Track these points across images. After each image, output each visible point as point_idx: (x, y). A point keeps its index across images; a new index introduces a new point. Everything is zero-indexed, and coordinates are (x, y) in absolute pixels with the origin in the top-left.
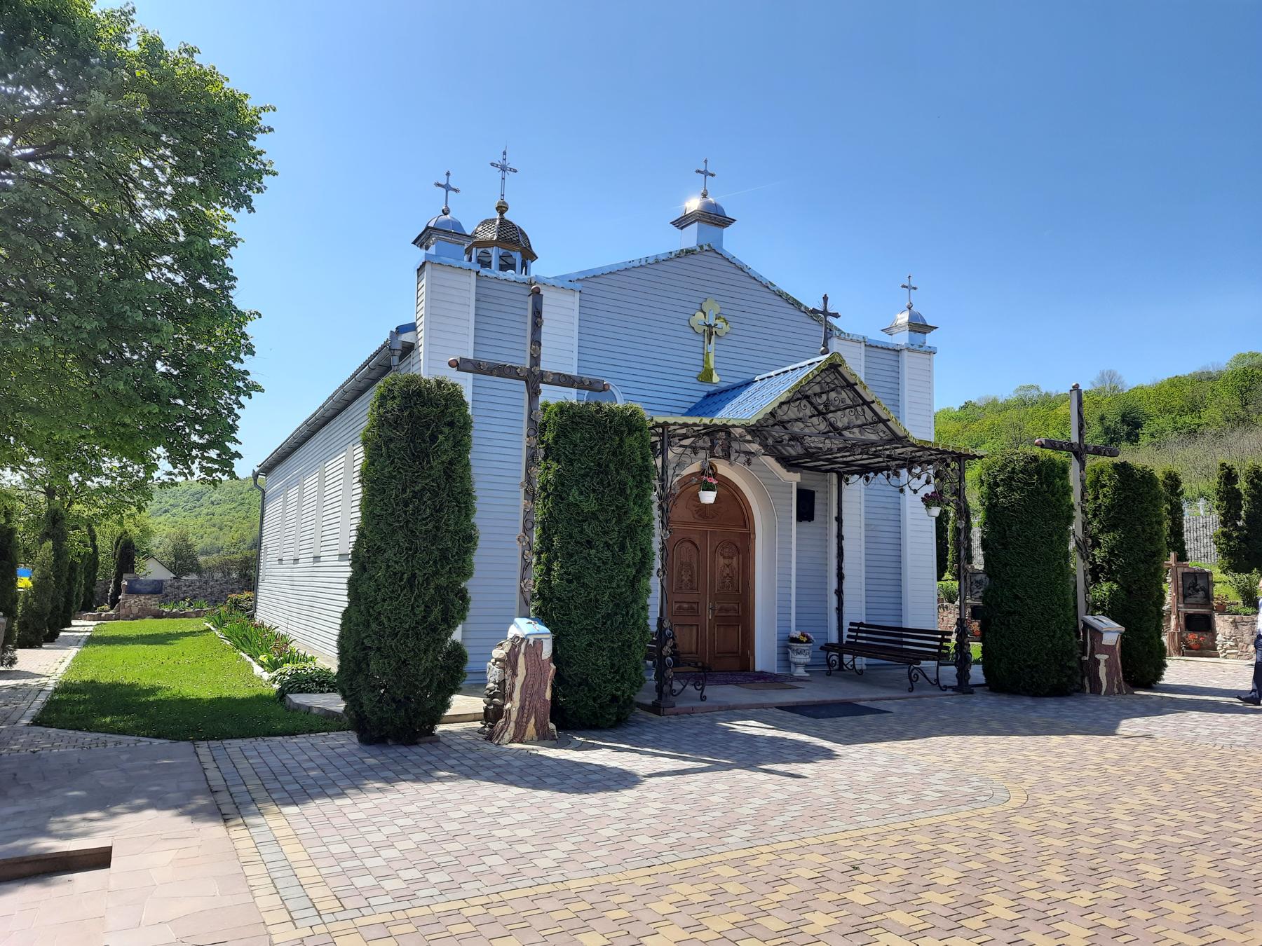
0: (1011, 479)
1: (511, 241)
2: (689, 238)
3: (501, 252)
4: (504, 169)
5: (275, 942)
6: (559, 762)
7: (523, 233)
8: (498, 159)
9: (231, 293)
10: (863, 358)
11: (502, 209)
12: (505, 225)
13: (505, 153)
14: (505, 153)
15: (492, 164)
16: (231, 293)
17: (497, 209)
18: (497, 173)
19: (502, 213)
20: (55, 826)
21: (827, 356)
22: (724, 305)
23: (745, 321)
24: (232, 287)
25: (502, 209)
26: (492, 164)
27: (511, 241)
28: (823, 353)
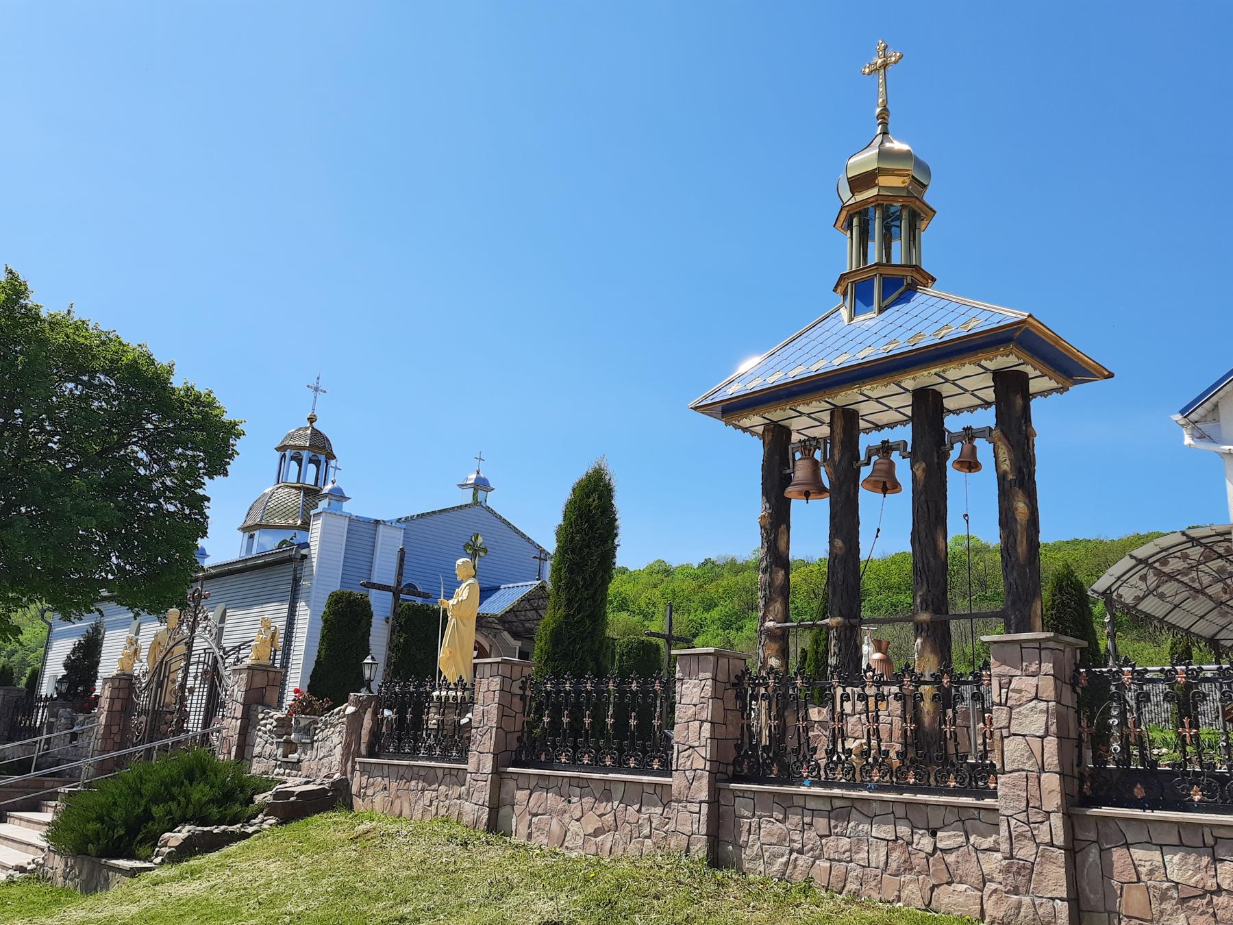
0: (630, 652)
1: (318, 448)
2: (466, 497)
3: (311, 454)
4: (316, 389)
5: (1132, 850)
6: (14, 742)
7: (328, 440)
8: (313, 383)
9: (227, 467)
10: (402, 539)
11: (312, 420)
12: (316, 433)
13: (318, 378)
14: (318, 378)
15: (308, 386)
16: (227, 467)
17: (308, 419)
18: (311, 392)
19: (311, 423)
20: (142, 851)
21: (540, 582)
22: (487, 538)
23: (427, 532)
24: (229, 464)
25: (312, 420)
26: (308, 386)
27: (318, 448)
28: (538, 580)
